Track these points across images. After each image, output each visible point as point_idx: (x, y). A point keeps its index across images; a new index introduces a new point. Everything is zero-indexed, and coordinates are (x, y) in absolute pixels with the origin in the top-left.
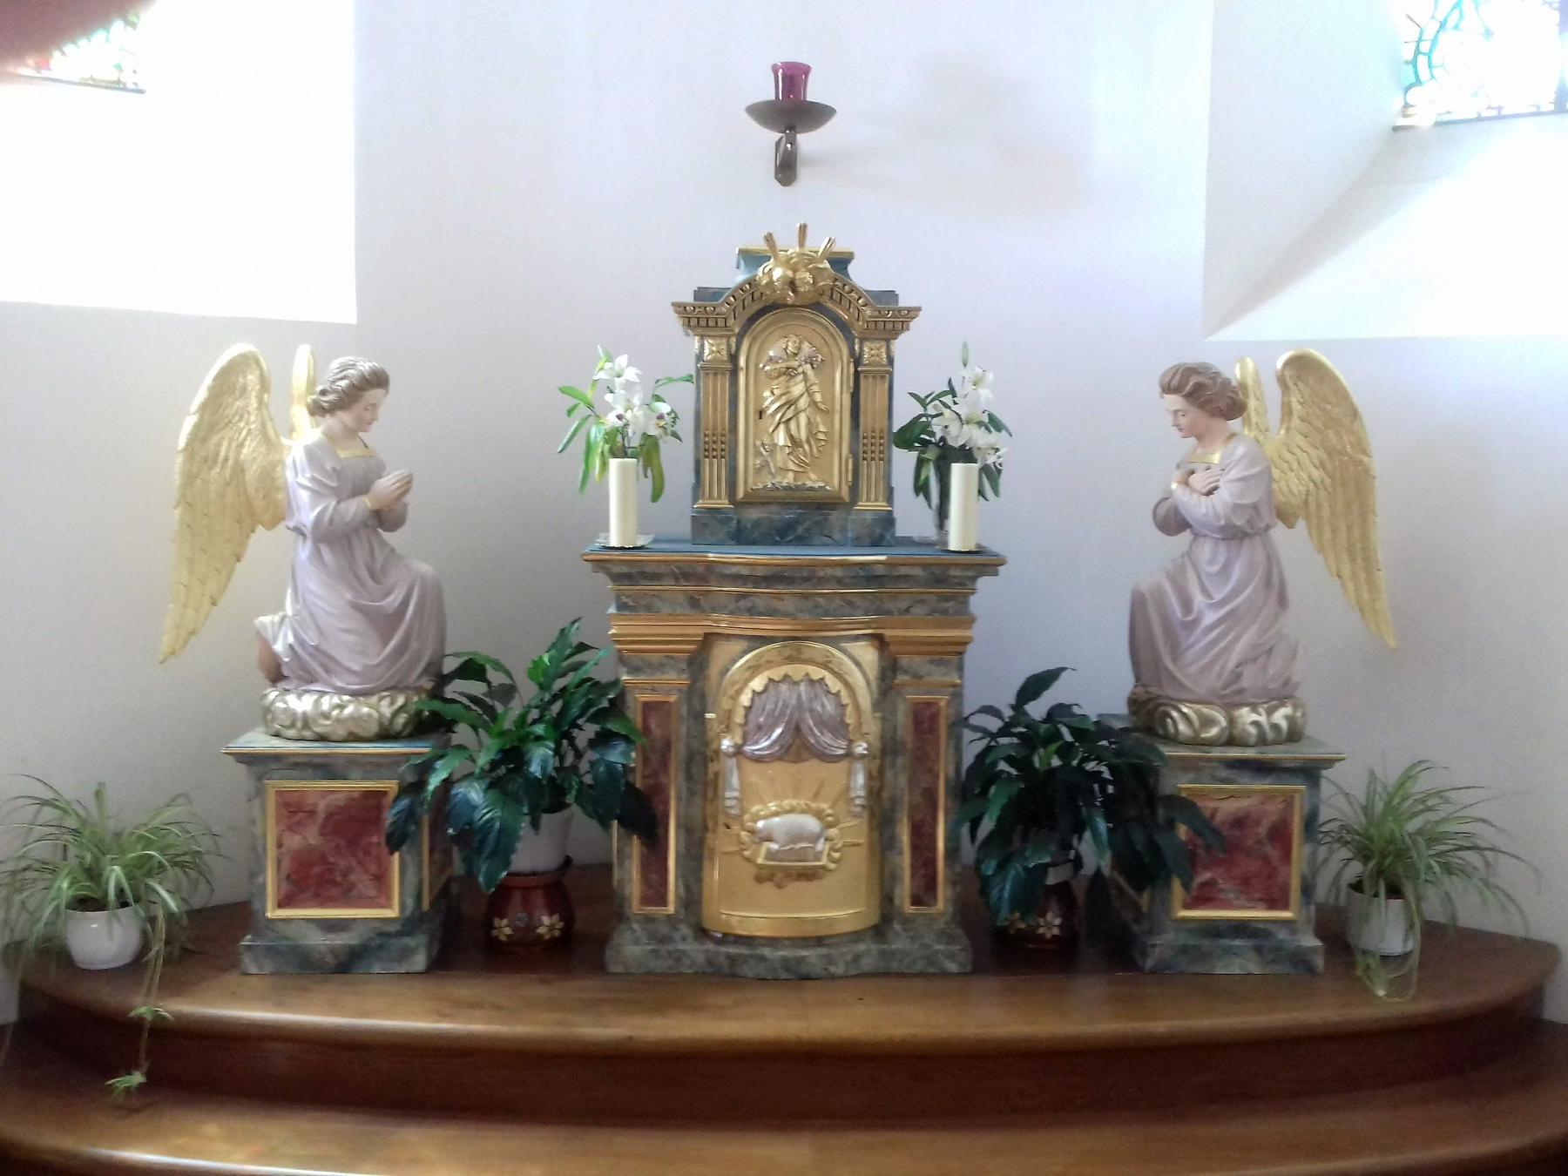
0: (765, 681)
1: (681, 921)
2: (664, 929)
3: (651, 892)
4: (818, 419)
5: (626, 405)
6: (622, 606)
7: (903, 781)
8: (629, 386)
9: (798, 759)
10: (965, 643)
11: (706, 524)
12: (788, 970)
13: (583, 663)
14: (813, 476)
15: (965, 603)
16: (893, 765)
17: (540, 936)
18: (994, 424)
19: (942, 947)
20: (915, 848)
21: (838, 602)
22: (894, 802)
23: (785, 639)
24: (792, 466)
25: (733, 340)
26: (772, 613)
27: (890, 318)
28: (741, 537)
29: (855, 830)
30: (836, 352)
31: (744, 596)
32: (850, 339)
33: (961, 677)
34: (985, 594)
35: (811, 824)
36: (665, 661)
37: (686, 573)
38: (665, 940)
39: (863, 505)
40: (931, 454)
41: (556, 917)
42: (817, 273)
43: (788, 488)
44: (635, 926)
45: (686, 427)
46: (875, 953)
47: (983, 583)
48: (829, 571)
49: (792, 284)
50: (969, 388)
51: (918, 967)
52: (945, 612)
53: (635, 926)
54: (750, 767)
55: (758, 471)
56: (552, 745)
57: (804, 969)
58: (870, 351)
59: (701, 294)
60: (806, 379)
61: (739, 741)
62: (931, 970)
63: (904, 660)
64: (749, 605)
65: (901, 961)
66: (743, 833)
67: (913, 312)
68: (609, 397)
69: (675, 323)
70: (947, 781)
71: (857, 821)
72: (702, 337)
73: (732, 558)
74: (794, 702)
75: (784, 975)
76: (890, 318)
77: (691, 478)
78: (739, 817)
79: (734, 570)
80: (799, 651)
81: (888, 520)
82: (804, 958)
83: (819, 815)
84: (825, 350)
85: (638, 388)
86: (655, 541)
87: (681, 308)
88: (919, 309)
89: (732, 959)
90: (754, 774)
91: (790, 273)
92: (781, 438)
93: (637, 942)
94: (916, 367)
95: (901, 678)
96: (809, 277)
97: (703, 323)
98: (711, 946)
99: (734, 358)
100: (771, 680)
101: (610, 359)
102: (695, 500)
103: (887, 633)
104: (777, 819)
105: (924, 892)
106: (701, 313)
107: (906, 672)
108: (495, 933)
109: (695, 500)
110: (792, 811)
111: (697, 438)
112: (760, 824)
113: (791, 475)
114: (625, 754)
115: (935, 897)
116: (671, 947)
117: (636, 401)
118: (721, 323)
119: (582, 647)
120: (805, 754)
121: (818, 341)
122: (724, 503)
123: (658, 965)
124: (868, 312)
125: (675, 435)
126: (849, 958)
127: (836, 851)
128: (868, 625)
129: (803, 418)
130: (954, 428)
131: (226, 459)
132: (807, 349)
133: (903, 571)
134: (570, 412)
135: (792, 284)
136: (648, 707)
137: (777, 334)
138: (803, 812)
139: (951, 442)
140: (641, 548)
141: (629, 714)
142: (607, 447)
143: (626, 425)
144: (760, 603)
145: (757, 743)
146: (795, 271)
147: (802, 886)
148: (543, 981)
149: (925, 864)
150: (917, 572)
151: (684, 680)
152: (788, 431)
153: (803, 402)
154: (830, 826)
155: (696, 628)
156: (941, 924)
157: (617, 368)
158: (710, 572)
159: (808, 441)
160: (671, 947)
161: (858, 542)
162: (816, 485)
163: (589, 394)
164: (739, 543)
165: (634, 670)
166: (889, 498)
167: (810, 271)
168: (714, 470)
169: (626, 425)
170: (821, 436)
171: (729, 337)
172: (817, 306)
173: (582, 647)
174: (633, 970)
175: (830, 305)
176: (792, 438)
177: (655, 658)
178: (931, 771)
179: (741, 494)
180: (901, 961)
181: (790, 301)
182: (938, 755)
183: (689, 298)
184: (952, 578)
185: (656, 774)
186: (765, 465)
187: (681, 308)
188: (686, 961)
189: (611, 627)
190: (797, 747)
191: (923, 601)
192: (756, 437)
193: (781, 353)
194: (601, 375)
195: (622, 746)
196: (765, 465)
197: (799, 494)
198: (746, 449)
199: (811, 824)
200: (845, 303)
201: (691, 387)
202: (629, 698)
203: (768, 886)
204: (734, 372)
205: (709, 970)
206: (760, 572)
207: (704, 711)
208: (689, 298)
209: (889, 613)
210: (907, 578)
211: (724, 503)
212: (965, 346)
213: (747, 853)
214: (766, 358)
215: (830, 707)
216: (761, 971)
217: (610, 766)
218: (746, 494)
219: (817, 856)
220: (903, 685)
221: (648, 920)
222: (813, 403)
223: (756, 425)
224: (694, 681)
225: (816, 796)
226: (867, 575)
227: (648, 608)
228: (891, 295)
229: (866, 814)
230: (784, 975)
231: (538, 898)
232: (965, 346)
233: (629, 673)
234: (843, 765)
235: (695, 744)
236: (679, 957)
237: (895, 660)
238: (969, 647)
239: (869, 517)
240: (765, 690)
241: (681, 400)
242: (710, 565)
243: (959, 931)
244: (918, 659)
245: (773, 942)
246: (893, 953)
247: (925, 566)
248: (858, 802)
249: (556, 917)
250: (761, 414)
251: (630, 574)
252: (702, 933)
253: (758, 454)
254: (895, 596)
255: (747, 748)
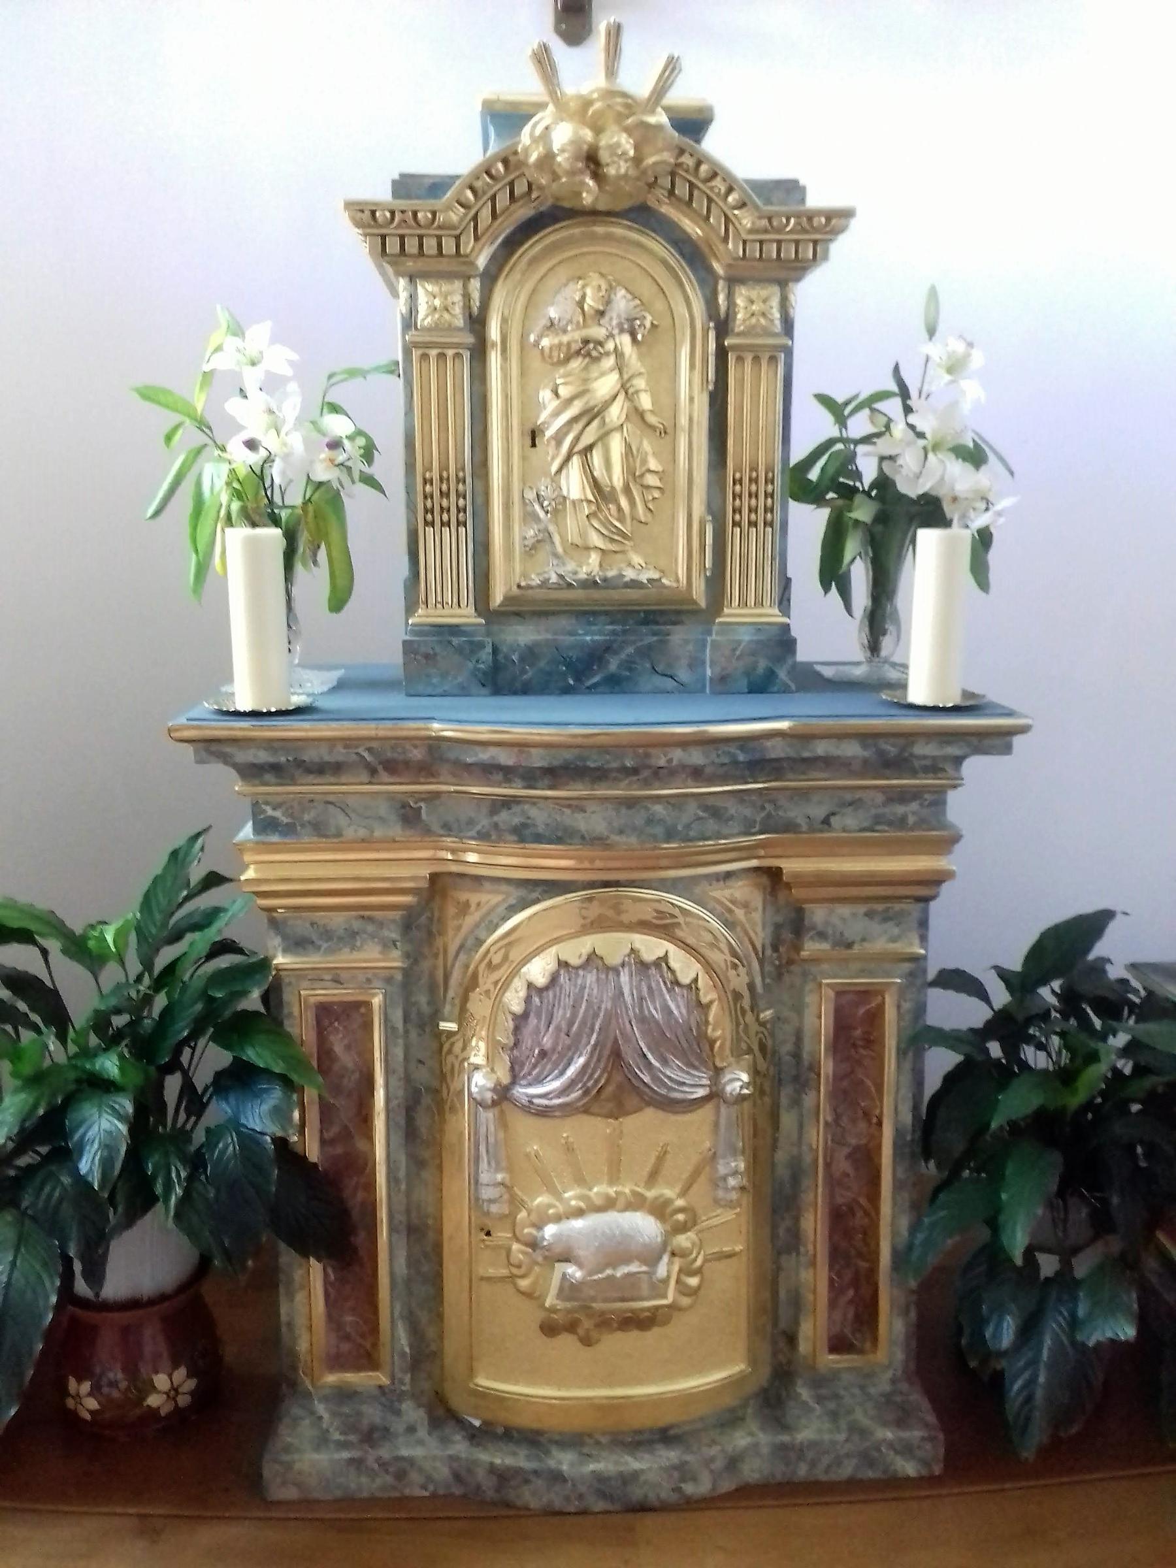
0: (552, 966)
1: (401, 1396)
2: (373, 1414)
3: (346, 1347)
4: (647, 446)
5: (276, 426)
6: (265, 826)
7: (817, 1137)
8: (272, 384)
9: (618, 1110)
10: (936, 880)
11: (433, 657)
12: (603, 1495)
13: (214, 913)
14: (637, 559)
15: (938, 802)
16: (796, 1102)
17: (153, 1412)
18: (975, 456)
19: (889, 1435)
20: (837, 1255)
21: (692, 808)
22: (797, 1172)
23: (592, 885)
24: (596, 540)
25: (475, 285)
26: (560, 836)
27: (793, 235)
28: (501, 679)
29: (728, 1227)
30: (680, 309)
31: (508, 803)
32: (707, 280)
33: (923, 939)
34: (978, 793)
35: (645, 1226)
36: (356, 925)
37: (388, 760)
38: (372, 1436)
39: (732, 613)
40: (863, 512)
41: (180, 1373)
42: (644, 135)
43: (590, 584)
44: (321, 1408)
45: (390, 466)
46: (765, 1450)
47: (975, 767)
48: (677, 755)
49: (592, 160)
50: (939, 380)
51: (847, 1470)
52: (901, 823)
53: (321, 1408)
54: (523, 1125)
55: (531, 550)
56: (129, 1107)
57: (637, 1493)
58: (749, 305)
59: (405, 185)
60: (620, 367)
61: (506, 1079)
62: (870, 1474)
63: (818, 915)
64: (516, 821)
65: (813, 1464)
66: (516, 1246)
67: (835, 221)
68: (234, 406)
69: (355, 247)
70: (899, 1133)
71: (729, 1215)
72: (412, 279)
73: (483, 732)
74: (607, 1004)
75: (600, 1506)
76: (793, 235)
77: (404, 569)
78: (509, 1219)
79: (485, 756)
80: (617, 908)
81: (784, 642)
82: (635, 1475)
83: (660, 1210)
84: (660, 305)
85: (293, 387)
86: (340, 686)
87: (366, 216)
88: (847, 214)
89: (503, 1476)
90: (533, 1139)
91: (588, 135)
92: (574, 484)
93: (322, 1441)
94: (842, 328)
95: (811, 947)
96: (627, 144)
97: (412, 246)
98: (460, 1447)
99: (477, 322)
100: (563, 964)
101: (237, 331)
102: (410, 609)
103: (790, 866)
104: (578, 1224)
105: (856, 1328)
106: (406, 230)
107: (822, 936)
108: (70, 1403)
109: (410, 609)
110: (609, 1204)
111: (410, 490)
112: (550, 1231)
113: (594, 558)
114: (280, 1114)
115: (875, 1340)
116: (385, 1452)
117: (291, 409)
118: (449, 246)
119: (214, 880)
120: (632, 1101)
121: (646, 289)
122: (466, 615)
123: (364, 1485)
124: (746, 220)
125: (370, 481)
126: (719, 1464)
127: (692, 1274)
128: (748, 852)
129: (616, 445)
130: (909, 460)
131: (770, 469)
132: (622, 303)
133: (821, 748)
134: (169, 438)
135: (592, 160)
136: (326, 1013)
137: (562, 273)
138: (630, 1206)
139: (904, 487)
140: (299, 711)
141: (291, 1027)
142: (236, 506)
143: (269, 460)
144: (539, 817)
145: (539, 1081)
146: (598, 131)
147: (632, 1339)
148: (148, 1530)
149: (855, 1283)
150: (852, 750)
151: (395, 960)
152: (587, 468)
153: (615, 413)
154: (682, 1228)
155: (408, 865)
156: (883, 1384)
157: (253, 352)
158: (435, 757)
159: (627, 490)
160: (385, 1452)
161: (723, 685)
162: (643, 578)
163: (199, 402)
164: (497, 691)
165: (297, 944)
166: (784, 602)
167: (628, 130)
168: (446, 550)
169: (269, 460)
170: (651, 480)
171: (467, 278)
172: (641, 215)
173: (214, 880)
174: (317, 1495)
175: (667, 210)
176: (596, 484)
177: (338, 921)
178: (867, 1115)
179: (498, 597)
180: (813, 1464)
181: (587, 199)
182: (879, 1087)
183: (381, 193)
184: (912, 762)
185: (346, 1135)
186: (545, 538)
187: (366, 216)
188: (415, 1476)
189: (245, 867)
190: (616, 1087)
191: (855, 804)
192: (523, 481)
193: (570, 309)
194: (220, 363)
195: (275, 1095)
196: (545, 538)
197: (615, 595)
198: (507, 506)
199: (645, 1226)
200: (700, 204)
201: (398, 385)
202: (288, 996)
203: (567, 1341)
204: (479, 352)
205: (457, 1491)
206: (538, 759)
207: (436, 1015)
208: (381, 193)
209: (790, 827)
210: (828, 763)
211: (466, 615)
212: (933, 294)
213: (524, 1283)
214: (544, 322)
215: (678, 1008)
216: (556, 1498)
217: (249, 1140)
218: (508, 599)
219: (659, 1288)
220: (815, 960)
221: (345, 1395)
222: (638, 414)
223: (524, 458)
224: (413, 958)
225: (653, 1177)
226: (751, 758)
227: (319, 828)
228: (792, 189)
229: (746, 1200)
230: (600, 1506)
231: (152, 1340)
232: (933, 294)
233: (286, 951)
234: (707, 1112)
235: (422, 1075)
236: (401, 1469)
237: (800, 911)
238: (945, 888)
239: (746, 637)
240: (554, 979)
241: (382, 409)
242: (435, 745)
243: (917, 1397)
244: (845, 910)
245: (575, 1441)
246: (800, 1451)
247: (866, 737)
248: (732, 1182)
249: (180, 1373)
250: (534, 436)
251: (278, 762)
252: (443, 1414)
253: (530, 517)
254: (803, 795)
255: (522, 1092)
